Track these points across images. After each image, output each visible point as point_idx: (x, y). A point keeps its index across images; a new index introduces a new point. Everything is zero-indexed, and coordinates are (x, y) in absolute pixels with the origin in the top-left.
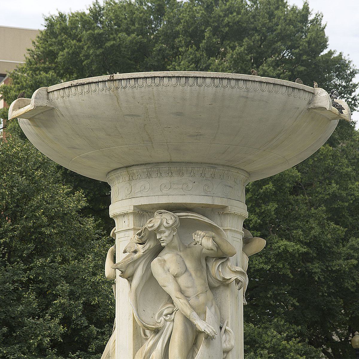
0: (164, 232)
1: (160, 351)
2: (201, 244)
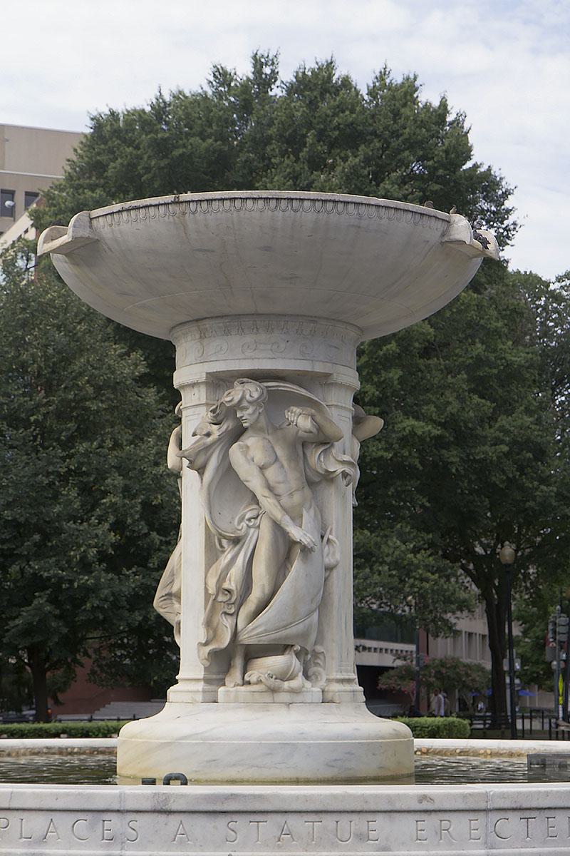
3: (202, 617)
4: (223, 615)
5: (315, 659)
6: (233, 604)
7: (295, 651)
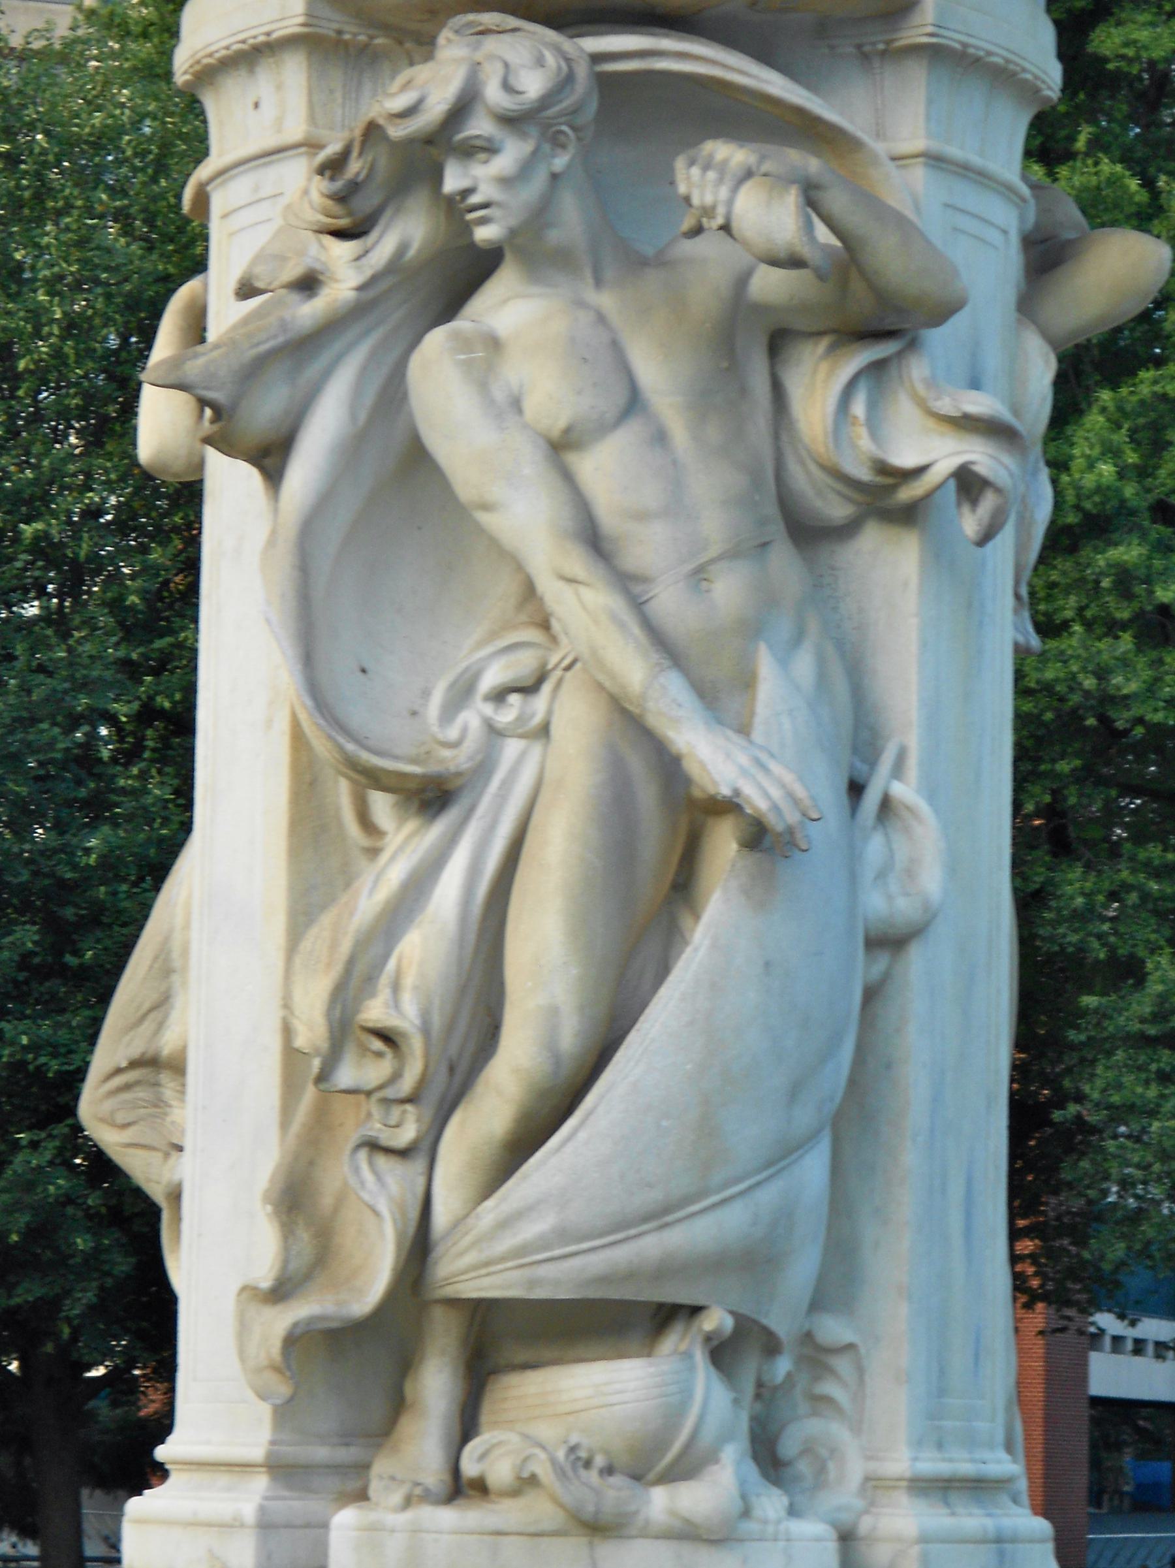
0: (490, 149)
2: (726, 228)
4: (363, 1155)
5: (816, 1379)
6: (409, 1100)
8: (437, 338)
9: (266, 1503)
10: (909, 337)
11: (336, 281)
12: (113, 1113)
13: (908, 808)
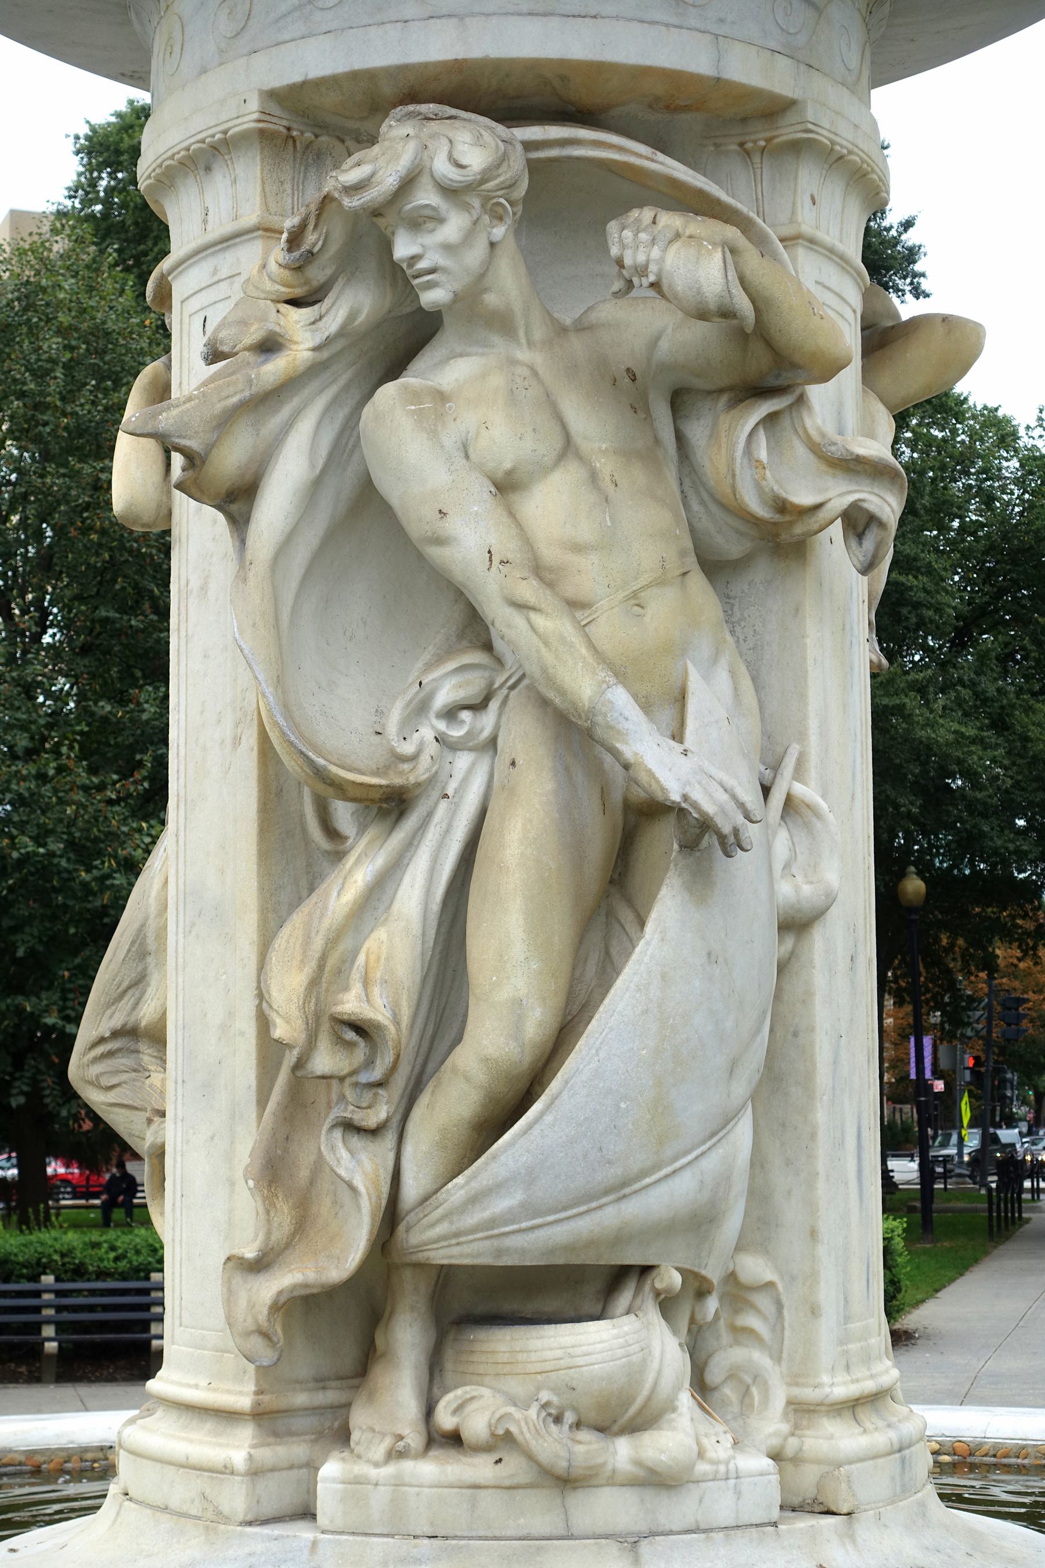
1: (416, 927)
3: (247, 1141)
4: (338, 1134)
5: (737, 1311)
6: (379, 1084)
7: (657, 1294)
8: (389, 391)
9: (252, 1451)
10: (797, 393)
11: (296, 343)
12: (97, 1077)
13: (808, 806)
